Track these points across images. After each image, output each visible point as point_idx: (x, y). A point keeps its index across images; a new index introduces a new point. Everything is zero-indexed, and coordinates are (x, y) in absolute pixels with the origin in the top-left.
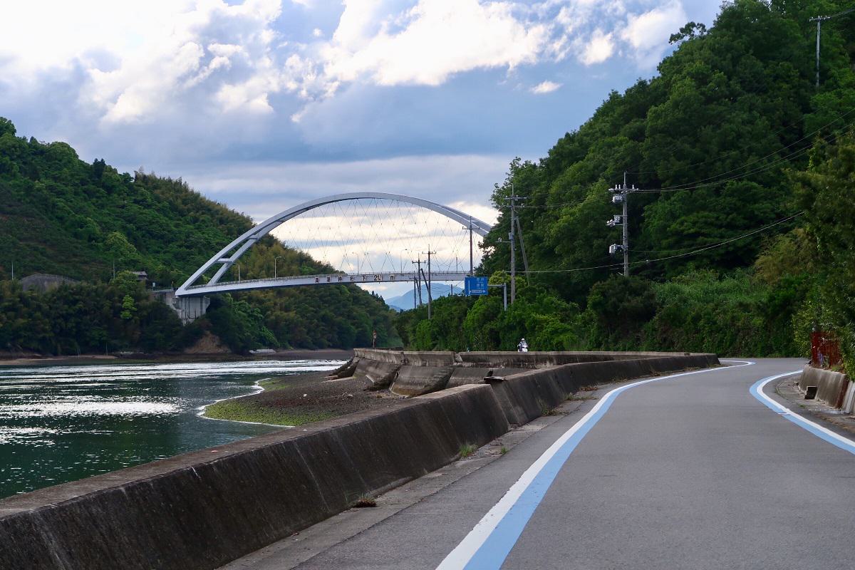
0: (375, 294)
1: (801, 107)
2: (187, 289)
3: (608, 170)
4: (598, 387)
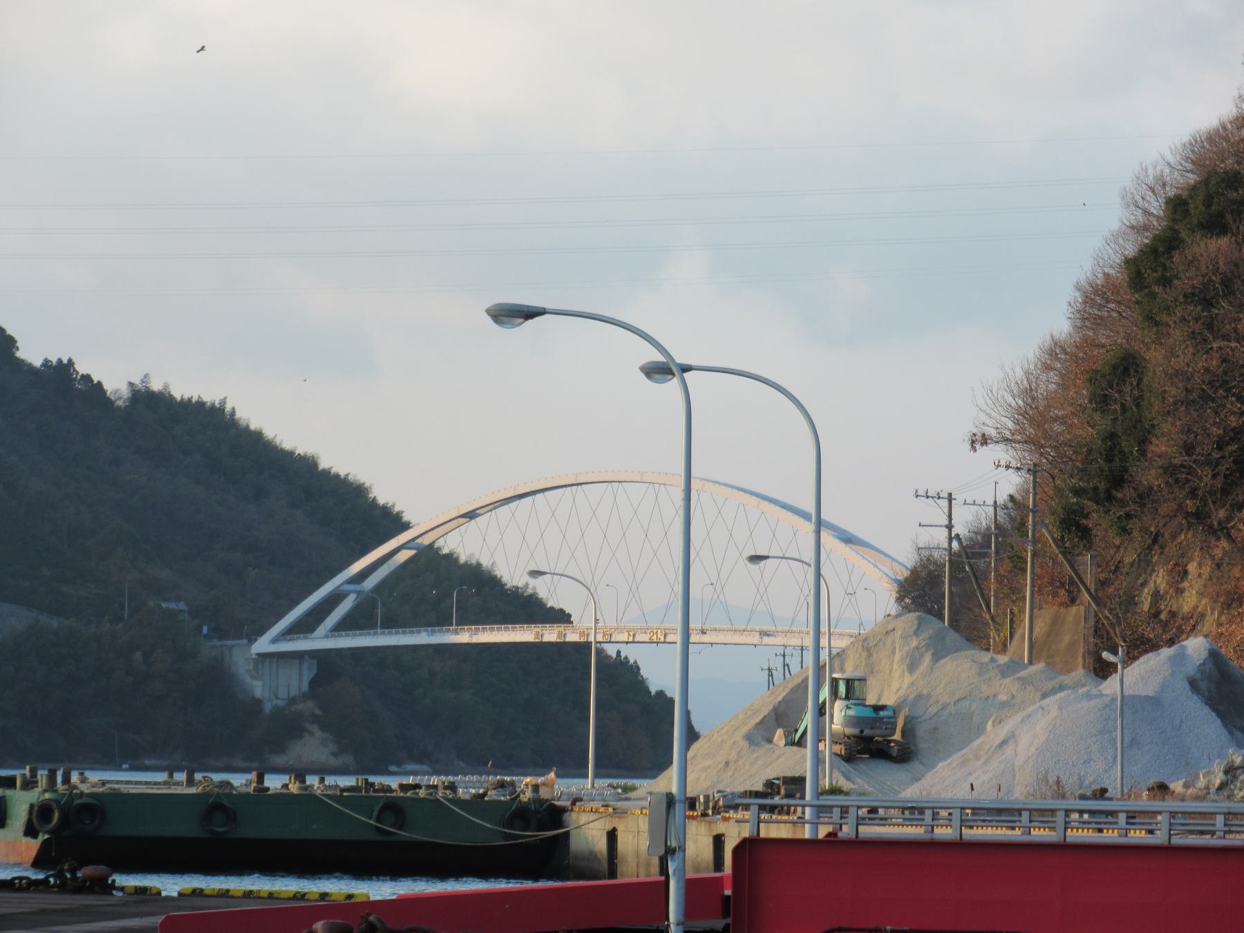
0: (623, 655)
1: (1228, 189)
2: (275, 641)
3: (883, 662)
4: (1239, 675)
